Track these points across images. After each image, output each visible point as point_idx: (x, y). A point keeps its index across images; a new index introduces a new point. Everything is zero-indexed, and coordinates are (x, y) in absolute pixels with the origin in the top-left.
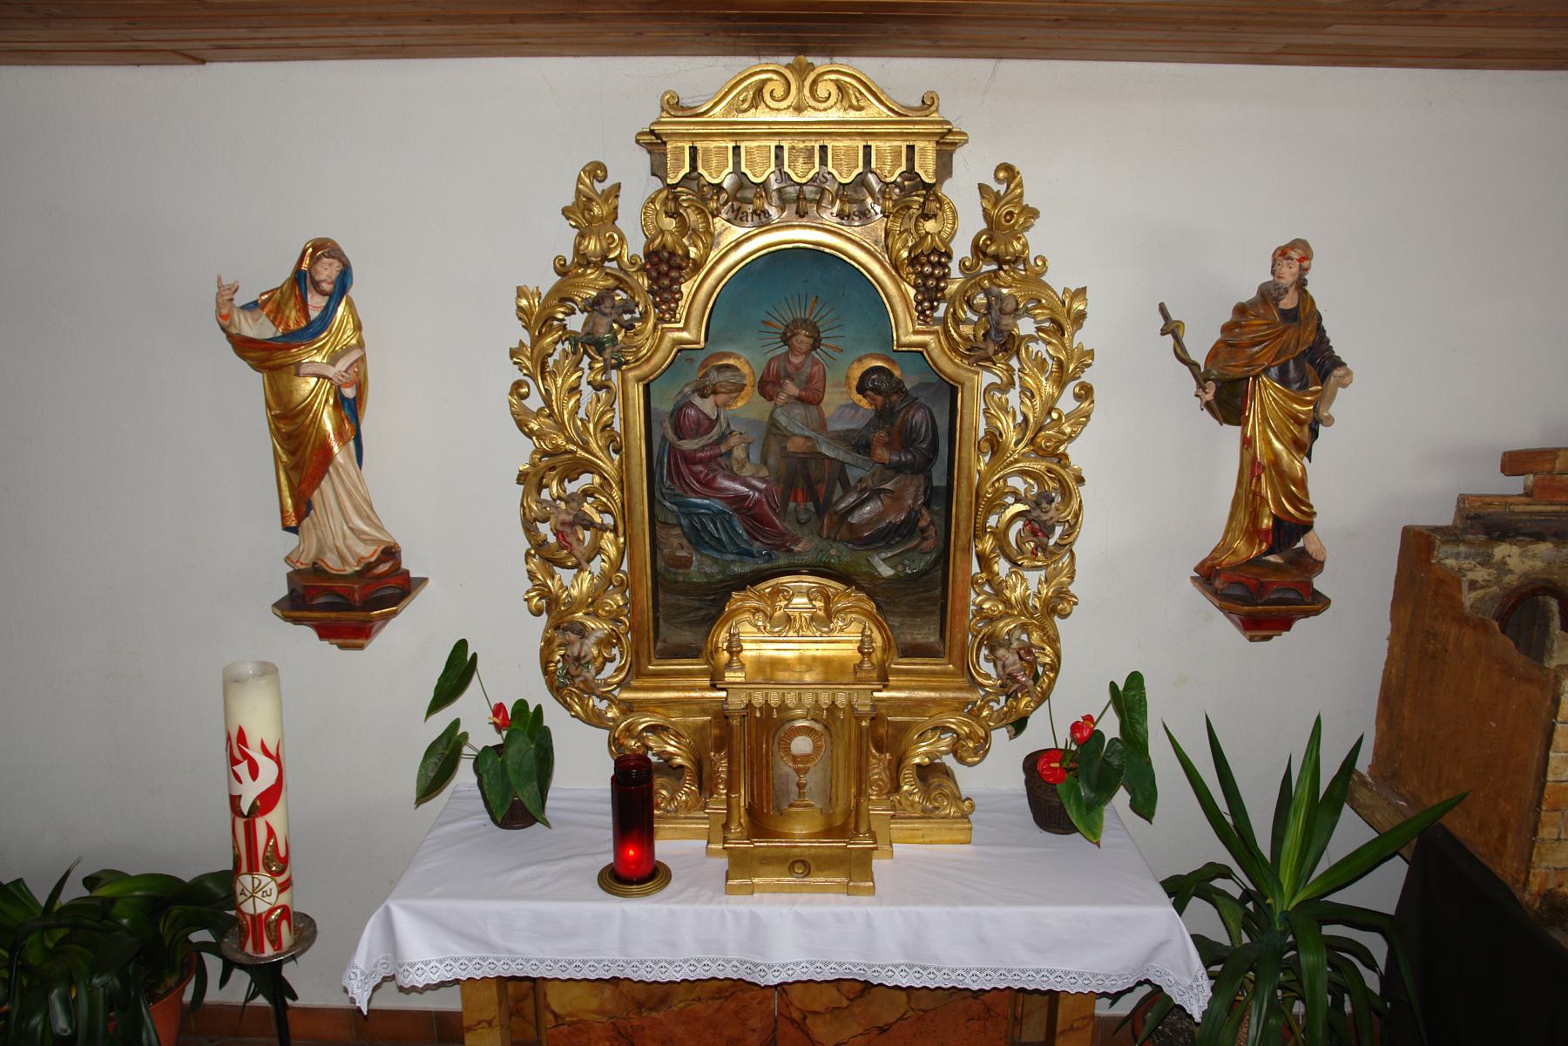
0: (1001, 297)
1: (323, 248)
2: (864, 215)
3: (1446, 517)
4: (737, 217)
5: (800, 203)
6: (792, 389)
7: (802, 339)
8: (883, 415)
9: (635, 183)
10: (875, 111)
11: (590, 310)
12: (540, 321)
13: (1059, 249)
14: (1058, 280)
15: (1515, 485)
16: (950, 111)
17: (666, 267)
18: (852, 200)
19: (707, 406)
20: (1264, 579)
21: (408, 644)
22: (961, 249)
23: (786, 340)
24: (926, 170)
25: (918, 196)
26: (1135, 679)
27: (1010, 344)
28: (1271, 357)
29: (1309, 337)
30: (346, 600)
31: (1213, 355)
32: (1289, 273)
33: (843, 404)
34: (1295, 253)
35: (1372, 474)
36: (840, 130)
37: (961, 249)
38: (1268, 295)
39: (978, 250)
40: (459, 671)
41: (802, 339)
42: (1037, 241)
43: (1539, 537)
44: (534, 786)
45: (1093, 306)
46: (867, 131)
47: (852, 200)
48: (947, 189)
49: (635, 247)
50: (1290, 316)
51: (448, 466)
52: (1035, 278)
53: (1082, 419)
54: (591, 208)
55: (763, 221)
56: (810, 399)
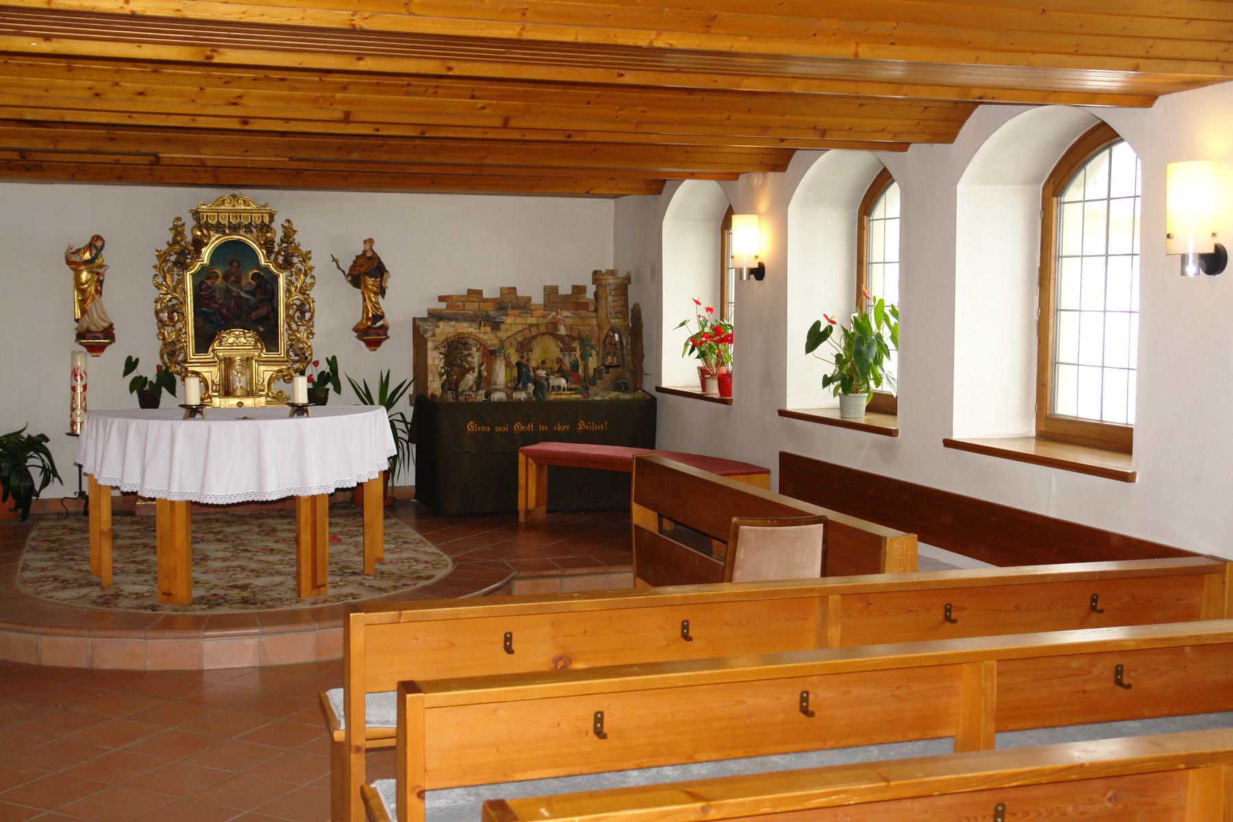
0: (289, 255)
1: (98, 238)
2: (251, 232)
3: (426, 315)
4: (217, 232)
5: (235, 229)
6: (233, 278)
7: (235, 264)
8: (258, 285)
9: (189, 222)
10: (253, 207)
11: (179, 254)
12: (163, 257)
13: (302, 240)
14: (304, 249)
15: (443, 305)
16: (272, 207)
17: (198, 244)
18: (248, 228)
19: (209, 282)
20: (372, 333)
21: (114, 356)
22: (277, 240)
23: (231, 264)
24: (267, 220)
25: (265, 228)
26: (334, 358)
27: (292, 264)
28: (368, 271)
29: (376, 264)
30: (95, 338)
31: (351, 269)
32: (368, 247)
33: (248, 280)
34: (370, 242)
35: (403, 303)
36: (244, 211)
37: (277, 240)
38: (365, 252)
39: (282, 241)
40: (131, 365)
41: (235, 264)
42: (297, 238)
43: (450, 320)
44: (211, 181)
45: (312, 255)
46: (250, 212)
47: (248, 228)
48: (273, 225)
49: (189, 238)
50: (370, 258)
51: (131, 302)
52: (297, 248)
53: (312, 284)
54: (177, 230)
55: (224, 234)
56: (238, 281)
